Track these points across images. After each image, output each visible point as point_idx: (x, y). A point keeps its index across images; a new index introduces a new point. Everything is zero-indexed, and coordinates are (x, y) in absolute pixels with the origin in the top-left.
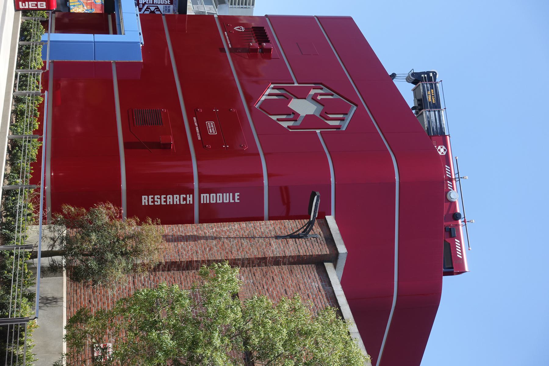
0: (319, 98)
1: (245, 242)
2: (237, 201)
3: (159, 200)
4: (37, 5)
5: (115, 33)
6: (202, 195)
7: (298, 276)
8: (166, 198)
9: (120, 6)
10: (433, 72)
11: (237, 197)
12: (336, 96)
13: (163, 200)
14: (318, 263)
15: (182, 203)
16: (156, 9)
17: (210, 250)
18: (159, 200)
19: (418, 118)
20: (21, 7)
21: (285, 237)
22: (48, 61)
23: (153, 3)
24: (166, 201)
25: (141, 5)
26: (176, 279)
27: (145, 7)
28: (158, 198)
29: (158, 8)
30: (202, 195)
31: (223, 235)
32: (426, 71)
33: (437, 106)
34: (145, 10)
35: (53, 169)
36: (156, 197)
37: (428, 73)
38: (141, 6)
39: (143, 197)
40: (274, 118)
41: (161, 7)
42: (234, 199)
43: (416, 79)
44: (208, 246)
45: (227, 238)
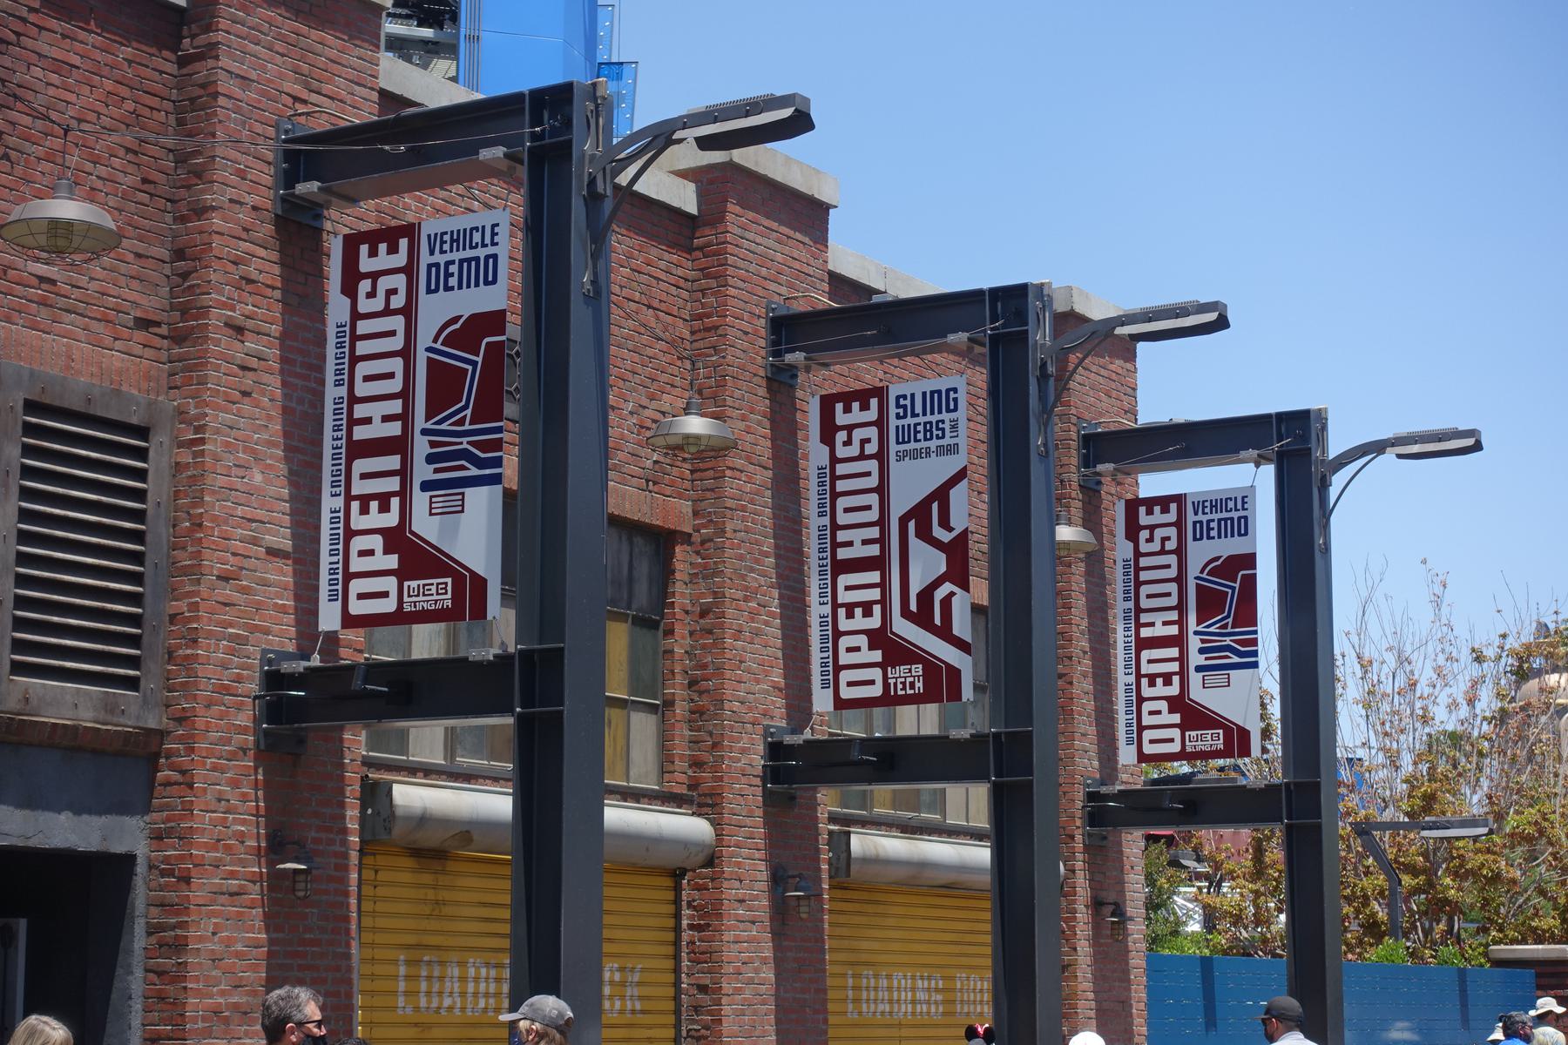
6: (406, 584)
16: (925, 534)
19: (613, 714)
23: (878, 563)
25: (899, 673)
27: (904, 628)
28: (1150, 540)
29: (920, 513)
30: (406, 584)
34: (945, 633)
38: (909, 676)
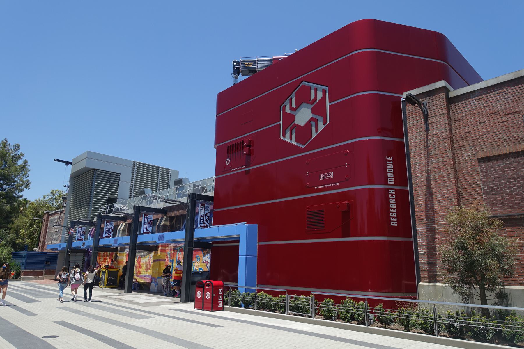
0: (294, 106)
1: (432, 153)
2: (391, 159)
3: (393, 213)
4: (221, 295)
5: (238, 241)
6: (389, 183)
7: (464, 115)
8: (392, 209)
9: (148, 243)
10: (234, 62)
11: (389, 159)
12: (293, 96)
13: (393, 211)
14: (451, 101)
15: (394, 197)
17: (442, 177)
18: (394, 214)
20: (221, 306)
21: (427, 124)
22: (257, 288)
24: (394, 209)
26: (470, 202)
30: (389, 183)
31: (425, 168)
32: (232, 67)
33: (255, 62)
35: (365, 290)
36: (391, 216)
37: (234, 66)
39: (392, 225)
40: (314, 135)
41: (206, 212)
42: (390, 161)
43: (237, 72)
44: (438, 179)
45: (428, 166)
